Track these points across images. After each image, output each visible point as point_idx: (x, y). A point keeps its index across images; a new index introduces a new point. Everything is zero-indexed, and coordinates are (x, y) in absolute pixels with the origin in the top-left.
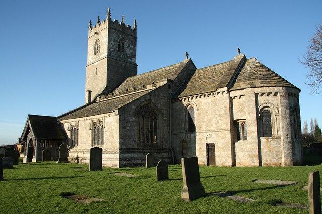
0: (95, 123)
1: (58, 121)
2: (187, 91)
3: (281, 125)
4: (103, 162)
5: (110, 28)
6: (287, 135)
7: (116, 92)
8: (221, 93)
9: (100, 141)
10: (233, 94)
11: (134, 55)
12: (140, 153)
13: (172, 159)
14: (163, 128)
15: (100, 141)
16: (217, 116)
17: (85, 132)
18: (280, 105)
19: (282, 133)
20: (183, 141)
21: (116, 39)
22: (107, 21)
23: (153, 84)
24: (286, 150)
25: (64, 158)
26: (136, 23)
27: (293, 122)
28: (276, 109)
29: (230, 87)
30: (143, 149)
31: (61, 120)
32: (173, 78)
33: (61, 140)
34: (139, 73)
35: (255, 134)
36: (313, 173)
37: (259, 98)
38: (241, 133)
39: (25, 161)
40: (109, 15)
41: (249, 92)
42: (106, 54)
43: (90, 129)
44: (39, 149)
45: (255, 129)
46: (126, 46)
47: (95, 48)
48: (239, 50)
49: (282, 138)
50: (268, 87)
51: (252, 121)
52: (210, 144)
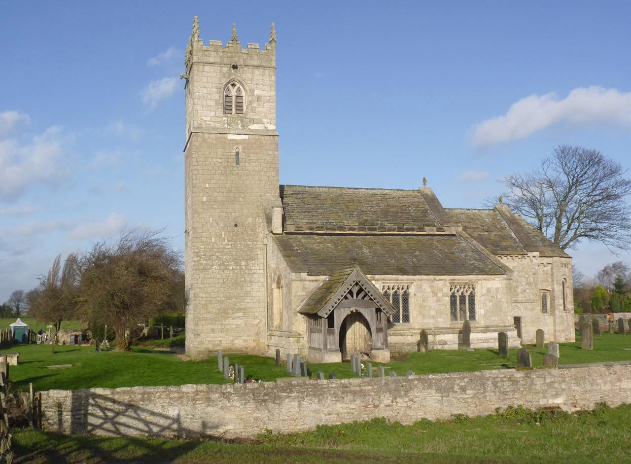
16: (524, 284)
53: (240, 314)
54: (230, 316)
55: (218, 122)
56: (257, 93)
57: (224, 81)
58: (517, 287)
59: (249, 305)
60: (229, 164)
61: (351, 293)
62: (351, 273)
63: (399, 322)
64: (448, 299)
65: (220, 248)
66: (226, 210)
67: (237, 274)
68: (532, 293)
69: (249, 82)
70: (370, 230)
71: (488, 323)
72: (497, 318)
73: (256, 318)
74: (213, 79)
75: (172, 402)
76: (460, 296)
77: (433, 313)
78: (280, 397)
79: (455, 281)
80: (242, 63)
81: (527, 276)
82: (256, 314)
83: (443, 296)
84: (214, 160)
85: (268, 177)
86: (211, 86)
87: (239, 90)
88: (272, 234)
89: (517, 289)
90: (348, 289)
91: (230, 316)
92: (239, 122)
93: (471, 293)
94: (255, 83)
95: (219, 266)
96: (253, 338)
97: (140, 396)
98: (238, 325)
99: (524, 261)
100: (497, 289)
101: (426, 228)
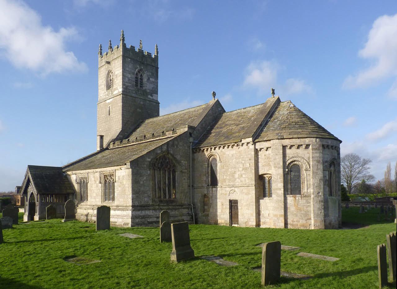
0: (105, 176)
1: (64, 172)
2: (211, 139)
3: (311, 181)
4: (111, 220)
5: (124, 57)
6: (319, 192)
7: (132, 138)
8: (246, 144)
9: (112, 196)
10: (258, 146)
11: (155, 91)
12: (155, 210)
13: (192, 216)
14: (182, 181)
15: (112, 196)
16: (241, 169)
17: (94, 186)
18: (311, 159)
19: (312, 191)
20: (205, 196)
21: (133, 71)
22: (121, 48)
23: (173, 130)
24: (316, 209)
25: (71, 216)
26: (157, 49)
27: (327, 178)
28: (307, 163)
29: (256, 136)
30: (159, 205)
31: (68, 171)
32: (196, 124)
33: (68, 194)
34: (161, 114)
35: (282, 191)
36: (266, 243)
37: (288, 151)
38: (267, 190)
39: (26, 219)
40: (123, 40)
41: (276, 144)
42: (121, 90)
43: (100, 183)
44: (42, 205)
45: (281, 185)
46: (145, 80)
47: (107, 82)
48: (273, 90)
49: (312, 196)
50: (299, 138)
51: (279, 177)
52: (233, 200)
58: (235, 172)
63: (46, 219)
68: (247, 177)
81: (243, 162)
89: (235, 175)
99: (242, 148)
101: (167, 133)
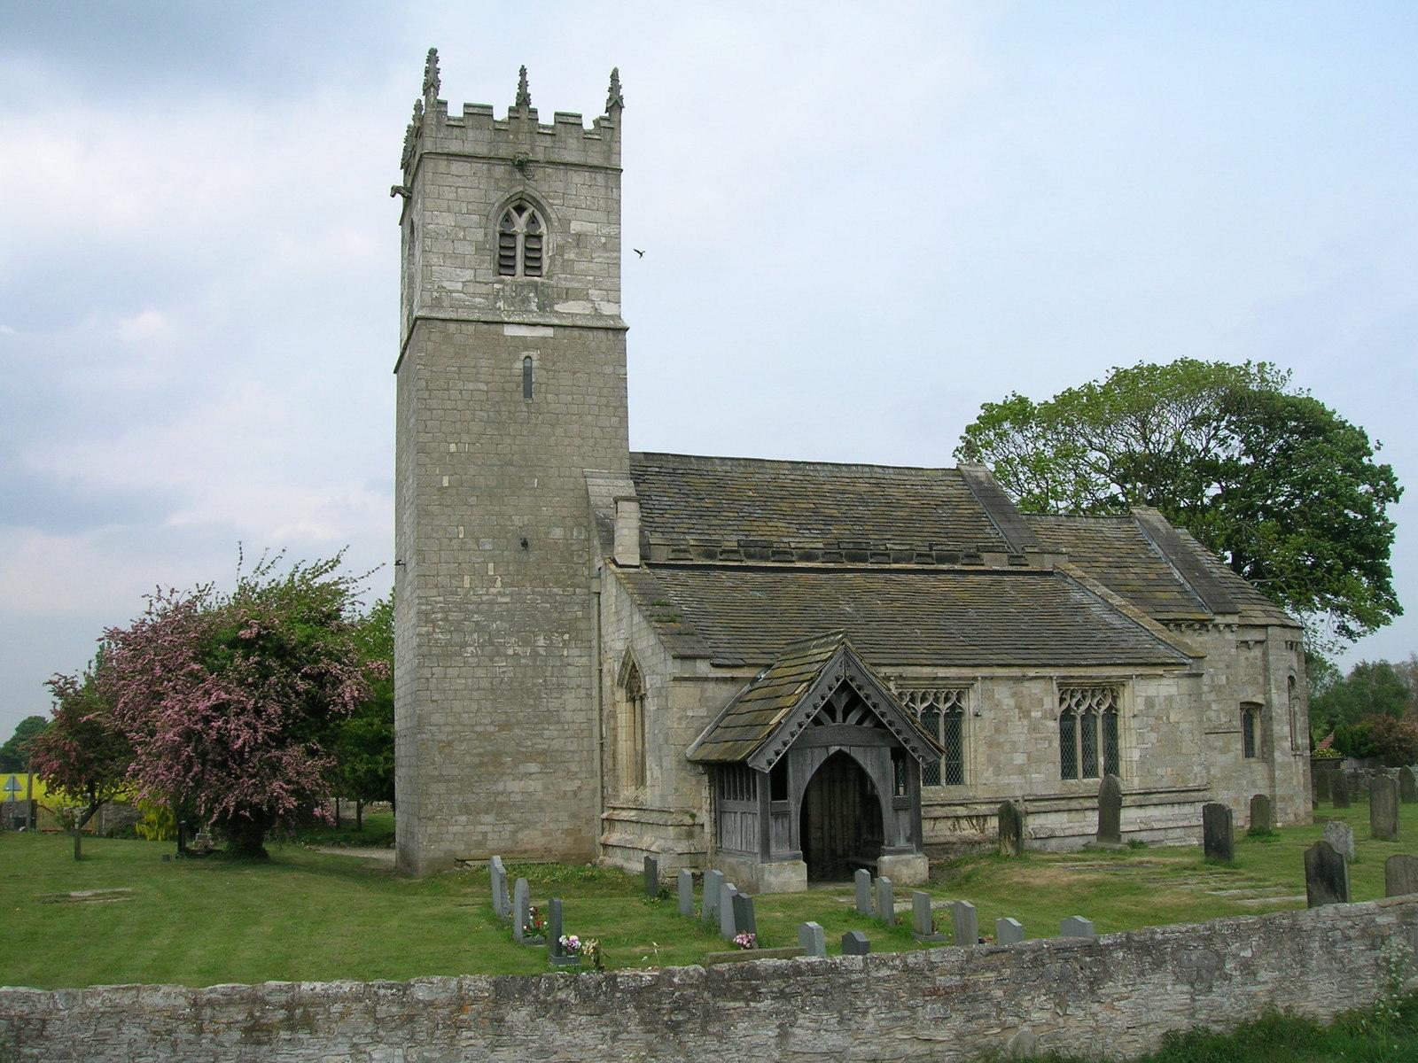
53: (533, 767)
54: (509, 771)
55: (480, 295)
56: (575, 227)
57: (497, 197)
59: (556, 745)
60: (507, 396)
61: (829, 709)
62: (831, 657)
64: (1054, 726)
65: (482, 603)
66: (497, 509)
67: (526, 666)
69: (556, 202)
70: (853, 559)
71: (1151, 784)
72: (1169, 769)
73: (571, 776)
74: (471, 191)
75: (382, 1033)
76: (1083, 718)
77: (1020, 759)
78: (719, 1014)
79: (1072, 681)
80: (540, 157)
82: (574, 767)
83: (1044, 717)
84: (471, 386)
85: (602, 428)
86: (465, 210)
87: (533, 220)
88: (613, 567)
90: (823, 698)
91: (509, 771)
92: (531, 295)
93: (1110, 708)
94: (572, 203)
95: (482, 646)
96: (566, 826)
97: (281, 1014)
98: (530, 794)
100: (1169, 699)
